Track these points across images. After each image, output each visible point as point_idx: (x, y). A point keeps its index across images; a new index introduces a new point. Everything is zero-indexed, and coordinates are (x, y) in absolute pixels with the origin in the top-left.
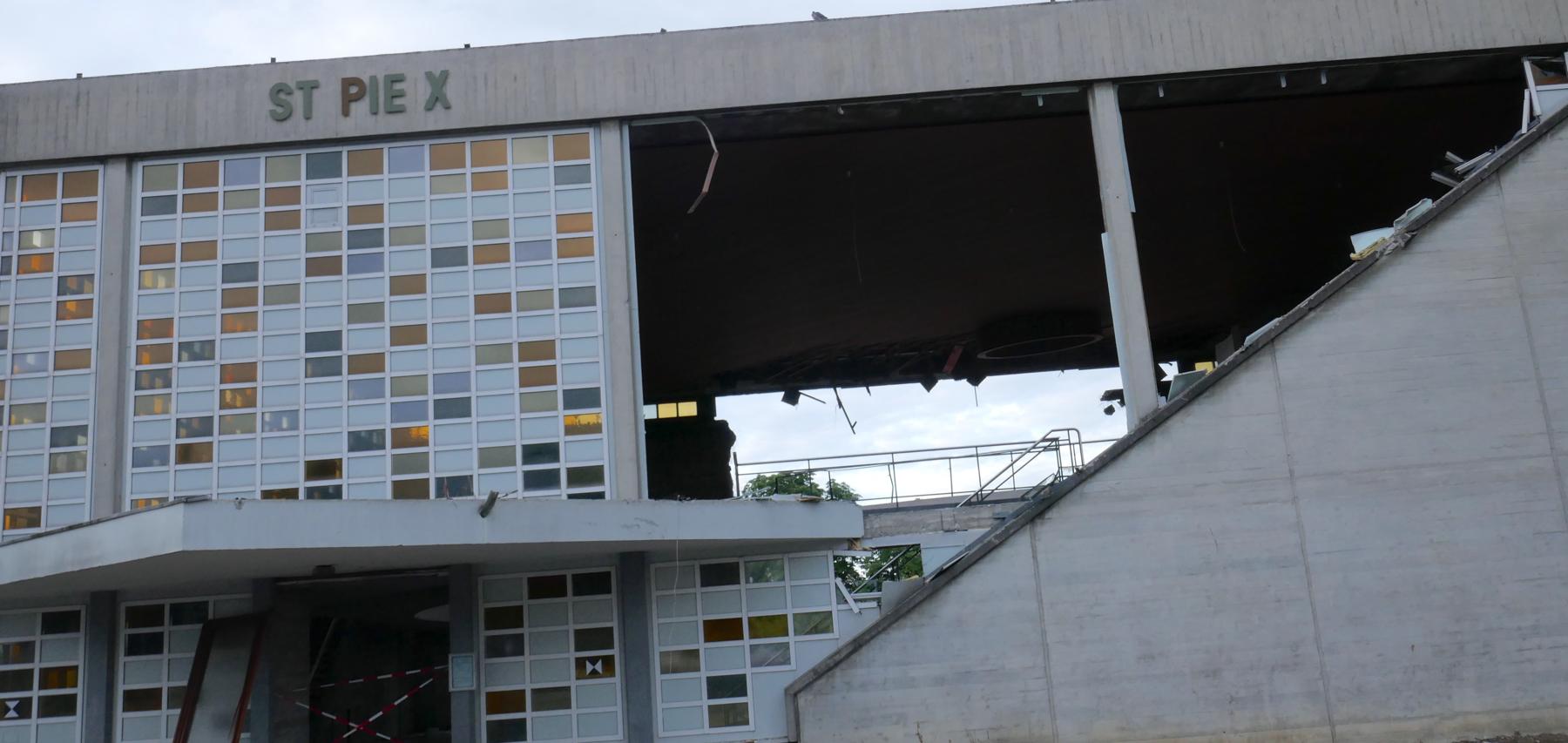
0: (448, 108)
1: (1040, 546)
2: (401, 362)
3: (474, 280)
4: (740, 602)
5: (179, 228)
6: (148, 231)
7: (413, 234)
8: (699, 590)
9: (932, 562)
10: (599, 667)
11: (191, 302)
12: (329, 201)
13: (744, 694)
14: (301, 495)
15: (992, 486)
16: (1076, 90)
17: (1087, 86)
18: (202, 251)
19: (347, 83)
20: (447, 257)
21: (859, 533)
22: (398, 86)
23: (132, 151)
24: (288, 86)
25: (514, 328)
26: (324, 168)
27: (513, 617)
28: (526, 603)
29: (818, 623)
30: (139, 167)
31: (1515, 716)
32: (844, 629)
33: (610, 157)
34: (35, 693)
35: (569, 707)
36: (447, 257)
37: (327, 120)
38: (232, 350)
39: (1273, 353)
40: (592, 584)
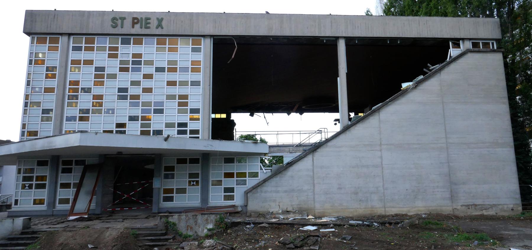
0: (162, 28)
1: (315, 158)
2: (145, 98)
3: (167, 76)
4: (235, 168)
5: (83, 56)
6: (73, 55)
7: (150, 63)
8: (223, 164)
9: (286, 161)
10: (195, 183)
11: (85, 76)
12: (127, 52)
13: (234, 192)
14: (114, 132)
15: (303, 142)
16: (334, 39)
17: (337, 38)
18: (89, 62)
19: (134, 19)
20: (160, 70)
21: (268, 152)
22: (148, 21)
23: (70, 32)
24: (117, 18)
25: (177, 91)
26: (126, 42)
27: (172, 169)
28: (176, 165)
29: (255, 175)
30: (72, 38)
31: (430, 208)
32: (261, 177)
33: (207, 46)
34: (34, 183)
35: (186, 193)
36: (160, 70)
37: (127, 28)
38: (97, 90)
39: (379, 112)
40: (194, 161)
